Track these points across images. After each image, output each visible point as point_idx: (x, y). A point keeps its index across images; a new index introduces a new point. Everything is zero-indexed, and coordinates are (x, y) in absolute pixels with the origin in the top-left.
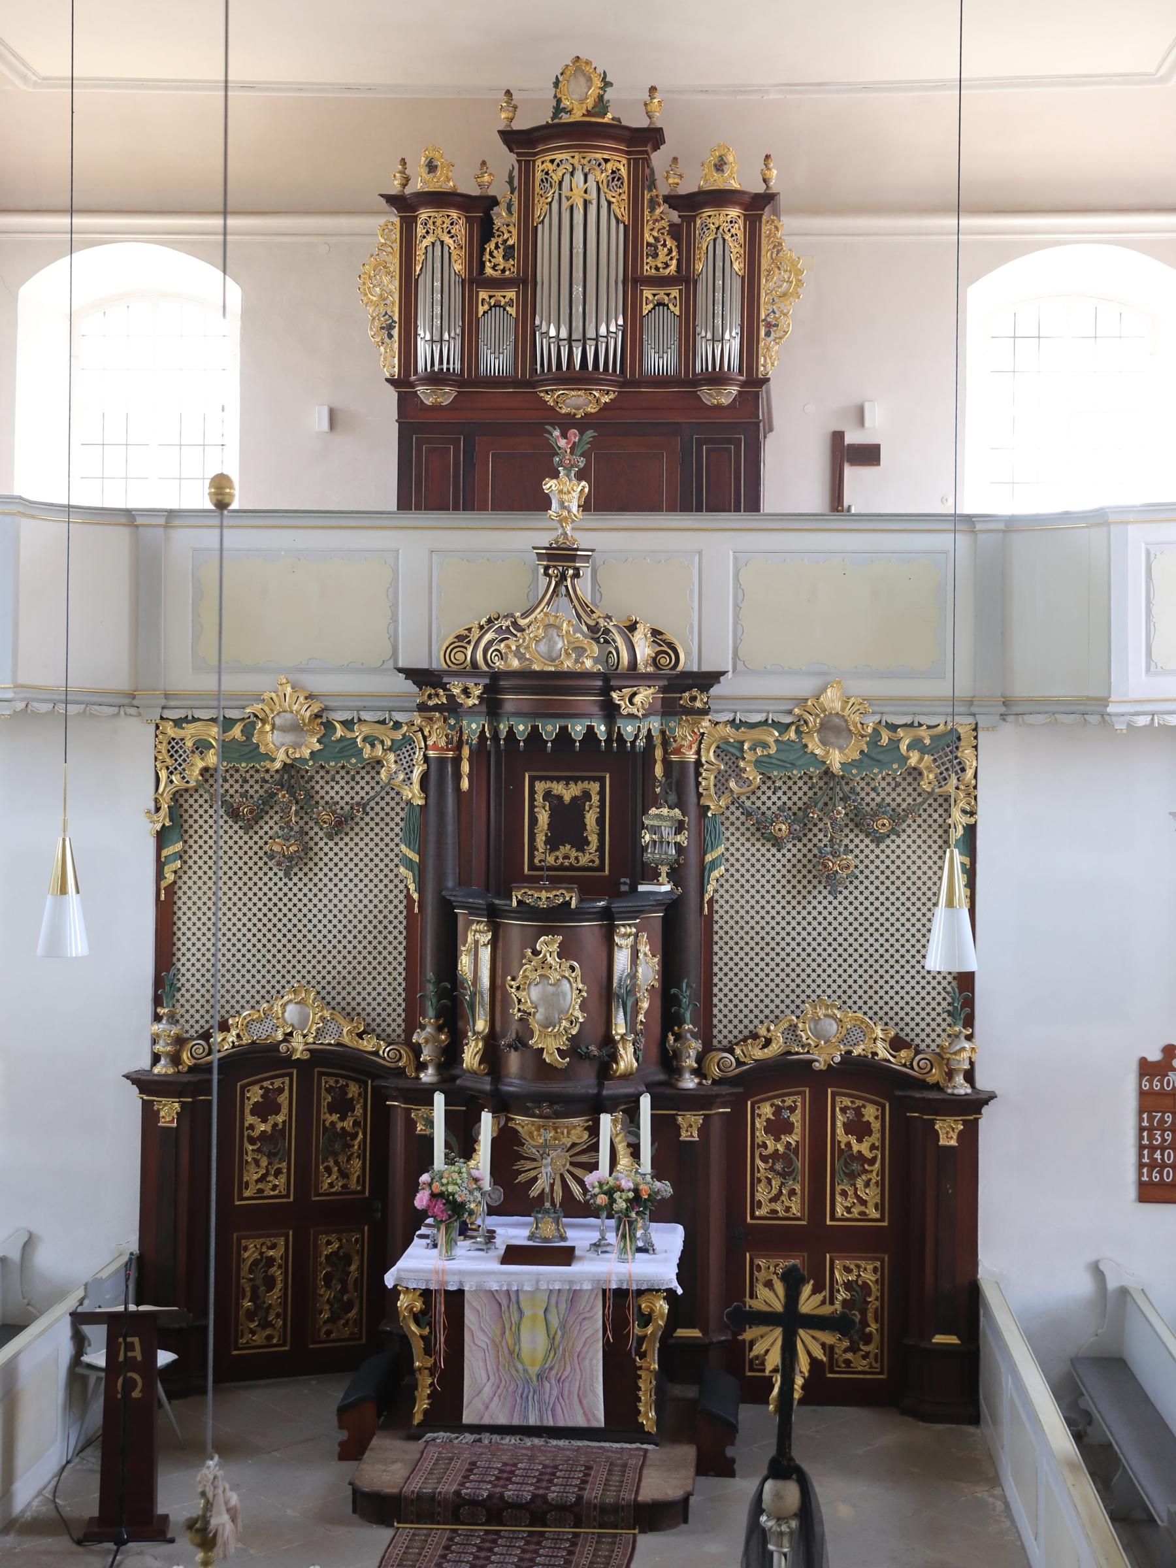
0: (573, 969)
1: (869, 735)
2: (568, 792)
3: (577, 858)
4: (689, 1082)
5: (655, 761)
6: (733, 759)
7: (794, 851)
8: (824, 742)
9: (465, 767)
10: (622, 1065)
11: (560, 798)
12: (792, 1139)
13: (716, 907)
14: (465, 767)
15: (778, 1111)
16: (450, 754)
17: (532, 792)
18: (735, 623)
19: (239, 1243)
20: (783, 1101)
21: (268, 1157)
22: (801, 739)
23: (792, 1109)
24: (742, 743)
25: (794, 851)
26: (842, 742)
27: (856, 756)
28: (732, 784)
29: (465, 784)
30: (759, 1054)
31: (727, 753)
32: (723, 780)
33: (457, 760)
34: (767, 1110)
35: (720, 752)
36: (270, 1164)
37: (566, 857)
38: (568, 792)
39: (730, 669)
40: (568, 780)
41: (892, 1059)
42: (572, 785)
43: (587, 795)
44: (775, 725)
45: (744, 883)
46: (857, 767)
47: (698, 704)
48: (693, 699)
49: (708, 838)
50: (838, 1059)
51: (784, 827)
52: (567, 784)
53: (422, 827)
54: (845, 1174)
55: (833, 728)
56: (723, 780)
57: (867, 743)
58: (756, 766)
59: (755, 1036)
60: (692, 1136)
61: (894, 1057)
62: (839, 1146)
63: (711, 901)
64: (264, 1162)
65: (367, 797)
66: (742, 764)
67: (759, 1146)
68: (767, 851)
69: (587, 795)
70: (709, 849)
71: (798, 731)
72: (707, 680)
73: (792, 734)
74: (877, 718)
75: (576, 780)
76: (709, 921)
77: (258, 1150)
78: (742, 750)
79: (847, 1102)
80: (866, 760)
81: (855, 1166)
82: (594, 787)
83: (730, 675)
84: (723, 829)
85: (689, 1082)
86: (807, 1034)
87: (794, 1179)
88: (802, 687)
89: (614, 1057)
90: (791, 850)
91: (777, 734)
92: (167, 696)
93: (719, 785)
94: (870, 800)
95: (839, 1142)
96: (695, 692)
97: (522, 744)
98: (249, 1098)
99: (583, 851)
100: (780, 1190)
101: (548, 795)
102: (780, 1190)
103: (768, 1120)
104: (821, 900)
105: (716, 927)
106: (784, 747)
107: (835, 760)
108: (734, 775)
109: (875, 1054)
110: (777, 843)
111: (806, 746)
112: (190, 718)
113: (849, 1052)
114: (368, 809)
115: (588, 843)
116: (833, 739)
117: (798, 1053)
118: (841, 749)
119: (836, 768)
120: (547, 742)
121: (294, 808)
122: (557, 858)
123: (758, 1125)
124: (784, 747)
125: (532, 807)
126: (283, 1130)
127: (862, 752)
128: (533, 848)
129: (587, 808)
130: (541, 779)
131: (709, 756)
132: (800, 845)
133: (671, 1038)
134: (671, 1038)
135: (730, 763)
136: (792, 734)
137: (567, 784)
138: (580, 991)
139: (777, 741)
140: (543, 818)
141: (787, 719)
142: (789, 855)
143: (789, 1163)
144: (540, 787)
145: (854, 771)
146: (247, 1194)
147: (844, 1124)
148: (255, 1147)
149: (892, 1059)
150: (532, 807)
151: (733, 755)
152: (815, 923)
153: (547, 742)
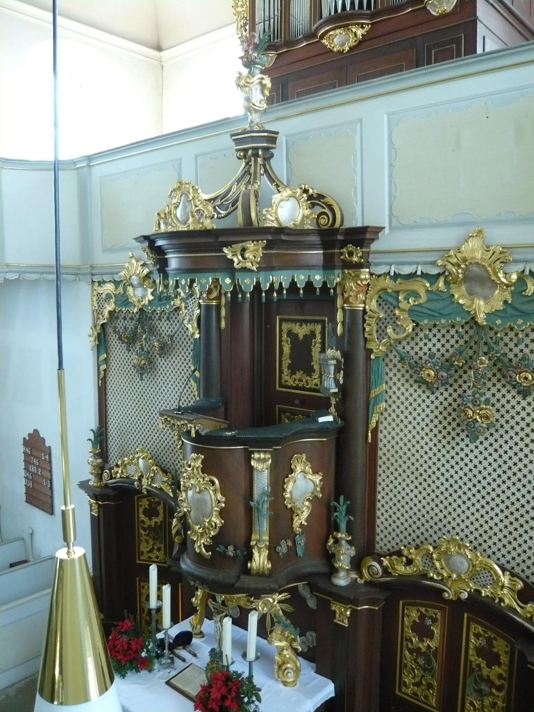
0: (213, 483)
1: (514, 284)
2: (301, 331)
3: (307, 381)
4: (342, 580)
5: (225, 318)
6: (392, 308)
7: (446, 394)
8: (471, 293)
9: (223, 313)
10: (254, 564)
11: (296, 335)
12: (433, 644)
13: (380, 436)
14: (223, 313)
15: (422, 617)
16: (214, 303)
17: (281, 331)
18: (390, 182)
19: (140, 585)
20: (426, 610)
21: (154, 539)
22: (449, 288)
23: (434, 620)
24: (398, 292)
25: (446, 394)
26: (486, 291)
27: (500, 306)
28: (389, 330)
29: (223, 324)
30: (401, 569)
31: (386, 302)
32: (383, 327)
33: (218, 307)
34: (414, 615)
35: (381, 301)
36: (154, 544)
37: (300, 380)
38: (301, 331)
39: (386, 224)
40: (302, 322)
41: (518, 609)
42: (304, 326)
43: (313, 334)
44: (424, 275)
45: (404, 421)
46: (501, 318)
47: (355, 259)
48: (351, 254)
49: (372, 377)
50: (465, 596)
51: (432, 373)
52: (301, 325)
53: (203, 355)
54: (475, 690)
55: (478, 278)
56: (383, 327)
57: (512, 293)
58: (410, 315)
59: (399, 554)
60: (343, 621)
61: (522, 608)
62: (471, 665)
63: (375, 431)
64: (151, 542)
65: (174, 331)
66: (397, 312)
67: (407, 640)
68: (417, 393)
69: (313, 334)
70: (373, 386)
71: (446, 283)
72: (362, 236)
73: (441, 284)
74: (520, 267)
75: (306, 322)
76: (373, 449)
77: (148, 535)
78: (398, 301)
79: (480, 630)
80: (510, 311)
81: (483, 686)
82: (318, 328)
83: (387, 231)
84: (387, 370)
85: (342, 580)
86: (441, 564)
87: (432, 676)
88: (444, 238)
89: (250, 557)
90: (444, 395)
91: (428, 285)
92: (92, 267)
93: (380, 331)
94: (513, 351)
95: (471, 662)
96: (351, 247)
97: (302, 292)
98: (141, 505)
99: (310, 376)
100: (421, 680)
101: (290, 333)
102: (421, 680)
103: (414, 621)
104: (466, 446)
105: (380, 453)
106: (434, 297)
107: (481, 308)
108: (391, 322)
109: (501, 600)
110: (430, 387)
111: (453, 296)
112: (419, 273)
113: (478, 592)
114: (174, 339)
115: (314, 371)
116: (478, 290)
117: (432, 579)
118: (486, 299)
119: (481, 318)
120: (330, 289)
121: (144, 336)
122: (295, 380)
123: (406, 623)
124: (434, 297)
125: (281, 341)
126: (160, 526)
127: (505, 302)
128: (281, 372)
129: (313, 344)
130: (287, 321)
131: (373, 305)
132: (451, 390)
133: (331, 541)
134: (331, 541)
135: (389, 311)
136: (441, 284)
137: (301, 325)
138: (219, 502)
139: (427, 291)
140: (287, 349)
141: (434, 271)
142: (441, 398)
143: (429, 662)
144: (285, 326)
145: (499, 322)
146: (142, 558)
147: (476, 648)
148: (146, 533)
149: (518, 609)
150: (281, 341)
151: (391, 304)
152: (481, 458)
153: (330, 289)
